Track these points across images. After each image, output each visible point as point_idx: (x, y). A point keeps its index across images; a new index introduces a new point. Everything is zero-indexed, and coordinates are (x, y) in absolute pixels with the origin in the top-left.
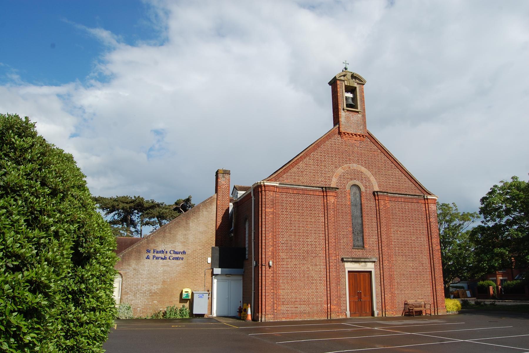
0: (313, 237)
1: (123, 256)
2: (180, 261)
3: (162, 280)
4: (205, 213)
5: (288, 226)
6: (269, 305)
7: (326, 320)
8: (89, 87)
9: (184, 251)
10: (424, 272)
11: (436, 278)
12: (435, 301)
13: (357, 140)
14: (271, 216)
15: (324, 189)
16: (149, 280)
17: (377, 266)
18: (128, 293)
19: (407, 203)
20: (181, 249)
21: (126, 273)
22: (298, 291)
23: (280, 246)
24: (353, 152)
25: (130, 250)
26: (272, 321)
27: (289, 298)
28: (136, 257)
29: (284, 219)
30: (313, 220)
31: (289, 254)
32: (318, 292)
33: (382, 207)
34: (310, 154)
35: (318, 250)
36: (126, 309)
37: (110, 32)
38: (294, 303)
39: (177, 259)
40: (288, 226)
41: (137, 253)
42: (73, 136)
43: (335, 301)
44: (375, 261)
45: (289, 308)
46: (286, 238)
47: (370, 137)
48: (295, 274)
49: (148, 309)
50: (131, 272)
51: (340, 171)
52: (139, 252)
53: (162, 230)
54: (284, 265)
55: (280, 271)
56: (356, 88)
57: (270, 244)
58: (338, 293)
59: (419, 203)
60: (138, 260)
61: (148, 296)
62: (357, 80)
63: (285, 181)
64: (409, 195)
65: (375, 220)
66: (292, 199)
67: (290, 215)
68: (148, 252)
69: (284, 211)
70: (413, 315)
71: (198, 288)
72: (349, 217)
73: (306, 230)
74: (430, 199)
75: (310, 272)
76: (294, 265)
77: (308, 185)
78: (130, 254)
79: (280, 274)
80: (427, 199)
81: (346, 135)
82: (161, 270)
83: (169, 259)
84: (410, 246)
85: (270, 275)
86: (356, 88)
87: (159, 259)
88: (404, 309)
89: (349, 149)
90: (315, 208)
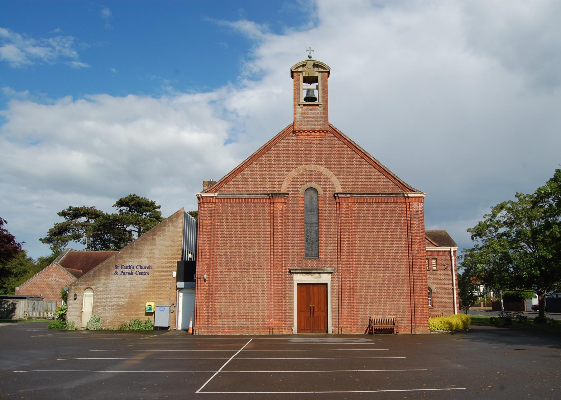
0: (256, 248)
1: (94, 272)
2: (147, 276)
3: (129, 294)
5: (228, 238)
8: (241, 88)
9: (150, 266)
10: (399, 283)
11: (416, 291)
13: (316, 138)
16: (117, 294)
17: (334, 277)
18: (98, 306)
19: (380, 204)
21: (96, 288)
22: (237, 304)
23: (218, 259)
24: (310, 151)
25: (100, 266)
26: (205, 334)
28: (105, 273)
29: (224, 230)
30: (257, 230)
31: (228, 267)
32: (260, 306)
33: (344, 210)
34: (257, 159)
35: (262, 262)
37: (253, 23)
39: (143, 273)
40: (228, 238)
41: (106, 269)
42: (228, 142)
44: (332, 272)
45: (226, 322)
47: (334, 131)
49: (116, 321)
50: (101, 287)
51: (293, 173)
52: (108, 268)
57: (206, 257)
58: (282, 308)
59: (397, 203)
60: (108, 275)
61: (116, 309)
62: (320, 68)
63: (227, 191)
64: (382, 194)
65: (334, 226)
66: (234, 209)
67: (230, 226)
68: (116, 267)
69: (224, 223)
70: (373, 334)
71: (163, 302)
72: (301, 224)
73: (248, 241)
74: (411, 197)
75: (251, 285)
78: (100, 270)
80: (408, 197)
82: (128, 284)
83: (136, 274)
84: (381, 254)
85: (205, 288)
86: (318, 77)
87: (126, 274)
89: (306, 148)
90: (261, 217)
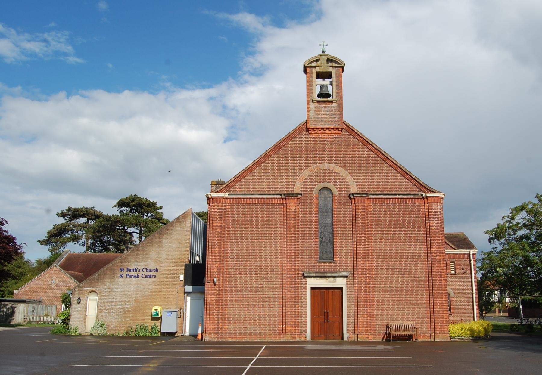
0: (268, 251)
2: (153, 279)
4: (179, 229)
5: (239, 240)
6: (212, 324)
7: (429, 341)
10: (418, 288)
12: (433, 324)
13: (331, 135)
14: (218, 230)
15: (283, 196)
17: (350, 281)
18: (103, 310)
20: (153, 267)
21: (101, 292)
22: (248, 309)
23: (228, 262)
25: (105, 269)
26: (215, 341)
27: (236, 317)
29: (235, 232)
30: (269, 232)
34: (269, 157)
35: (274, 265)
36: (100, 326)
38: (243, 322)
39: (150, 277)
40: (239, 240)
43: (292, 321)
44: (348, 276)
46: (236, 252)
47: (349, 129)
48: (245, 291)
49: (121, 326)
51: (307, 173)
53: (135, 249)
54: (232, 281)
55: (228, 288)
56: (332, 72)
57: (216, 260)
63: (238, 191)
64: (399, 194)
65: (349, 227)
66: (245, 210)
67: (241, 227)
69: (234, 224)
72: (314, 226)
73: (260, 243)
75: (263, 289)
76: (244, 281)
77: (266, 193)
78: (105, 273)
79: (228, 291)
80: (427, 198)
81: (316, 131)
82: (133, 288)
85: (215, 292)
86: (332, 72)
88: (386, 332)
89: (319, 147)
90: (273, 218)
